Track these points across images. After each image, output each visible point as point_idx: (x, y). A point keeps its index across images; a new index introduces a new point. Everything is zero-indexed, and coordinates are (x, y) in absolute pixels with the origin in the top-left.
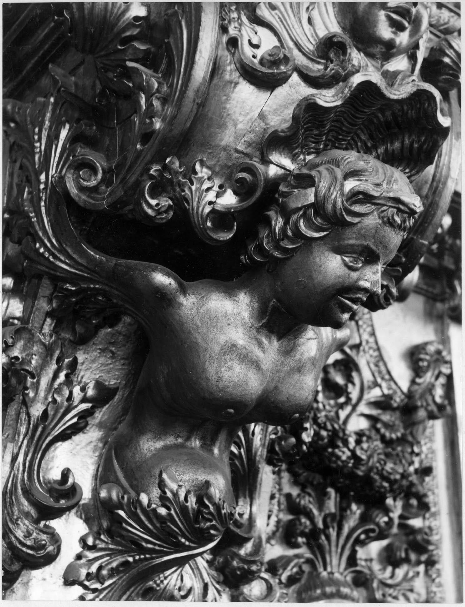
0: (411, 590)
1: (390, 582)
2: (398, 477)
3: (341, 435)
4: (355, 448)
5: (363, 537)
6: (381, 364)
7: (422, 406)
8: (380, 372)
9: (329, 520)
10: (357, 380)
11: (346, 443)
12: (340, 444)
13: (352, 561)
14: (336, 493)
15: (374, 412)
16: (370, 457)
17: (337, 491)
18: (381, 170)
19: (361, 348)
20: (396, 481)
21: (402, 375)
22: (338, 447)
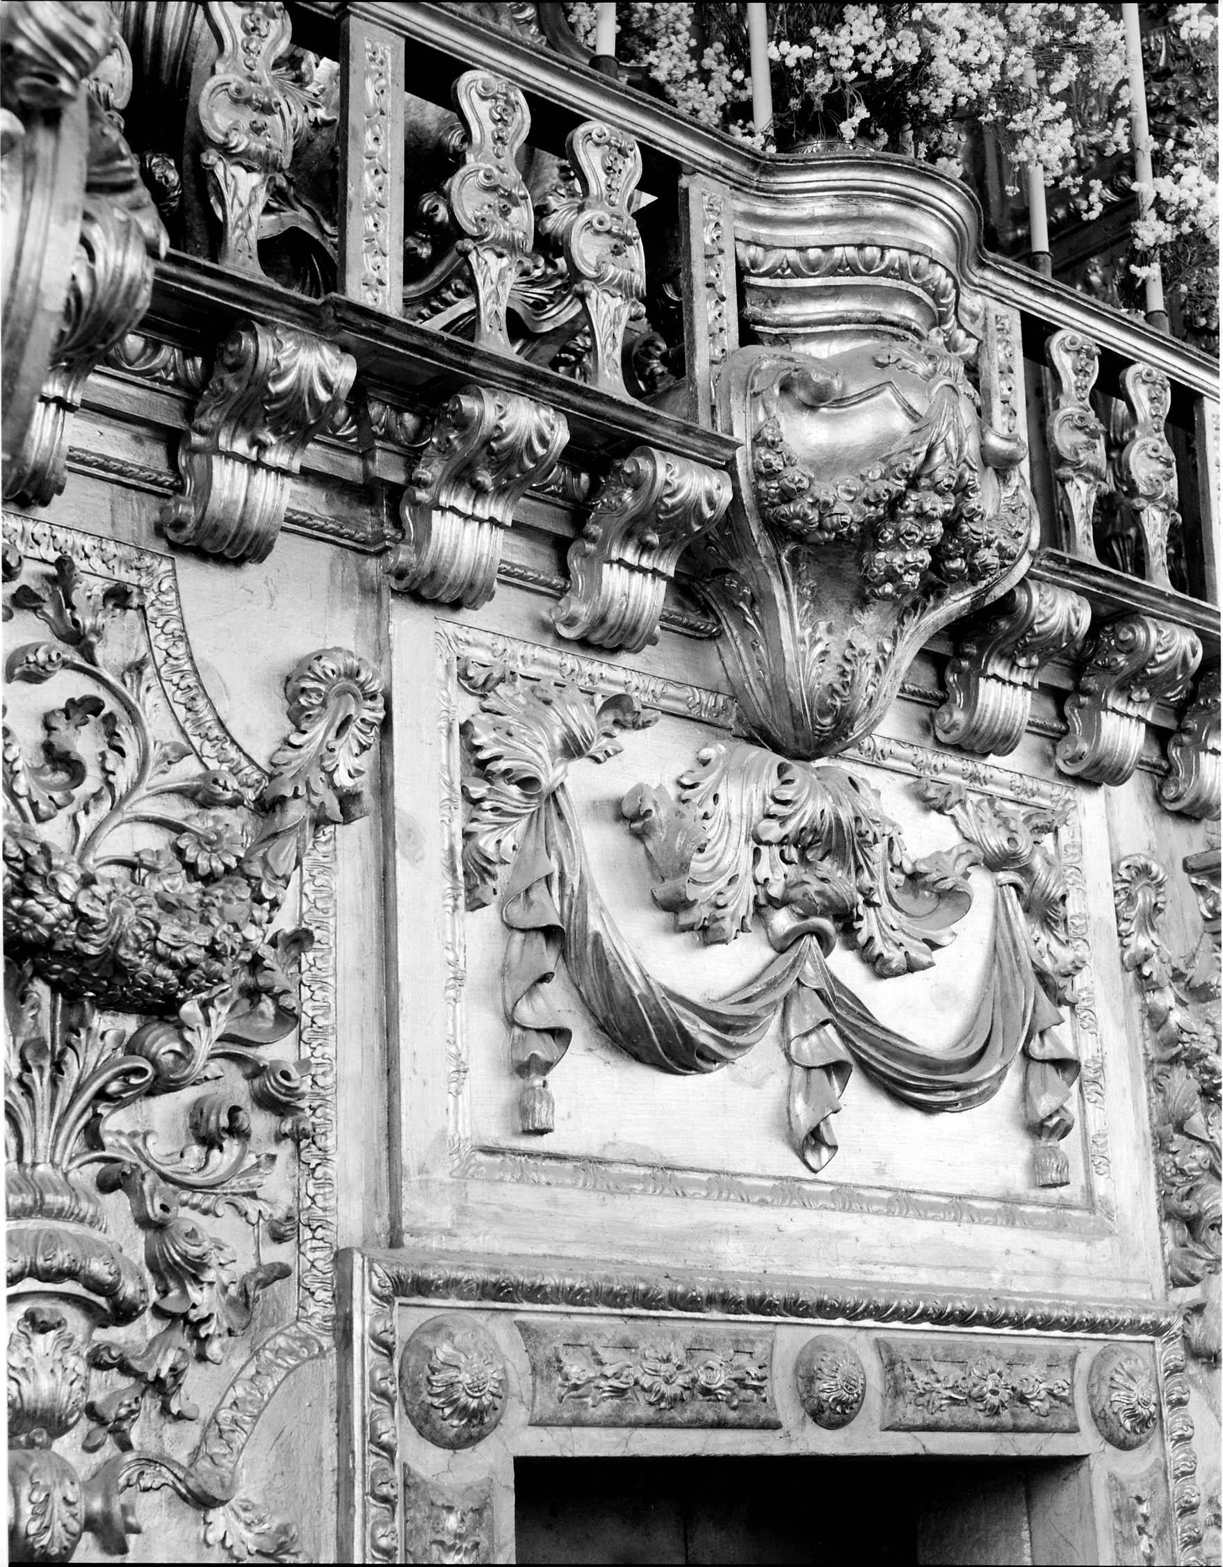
0: (253, 1195)
1: (195, 1179)
2: (195, 955)
3: (41, 868)
4: (76, 895)
5: (114, 1087)
6: (201, 703)
7: (296, 796)
8: (198, 723)
9: (29, 1054)
10: (129, 744)
11: (51, 884)
12: (37, 887)
13: (93, 1137)
14: (54, 993)
15: (177, 810)
16: (114, 915)
17: (56, 988)
18: (859, 772)
19: (149, 671)
20: (191, 965)
21: (258, 726)
22: (31, 894)
